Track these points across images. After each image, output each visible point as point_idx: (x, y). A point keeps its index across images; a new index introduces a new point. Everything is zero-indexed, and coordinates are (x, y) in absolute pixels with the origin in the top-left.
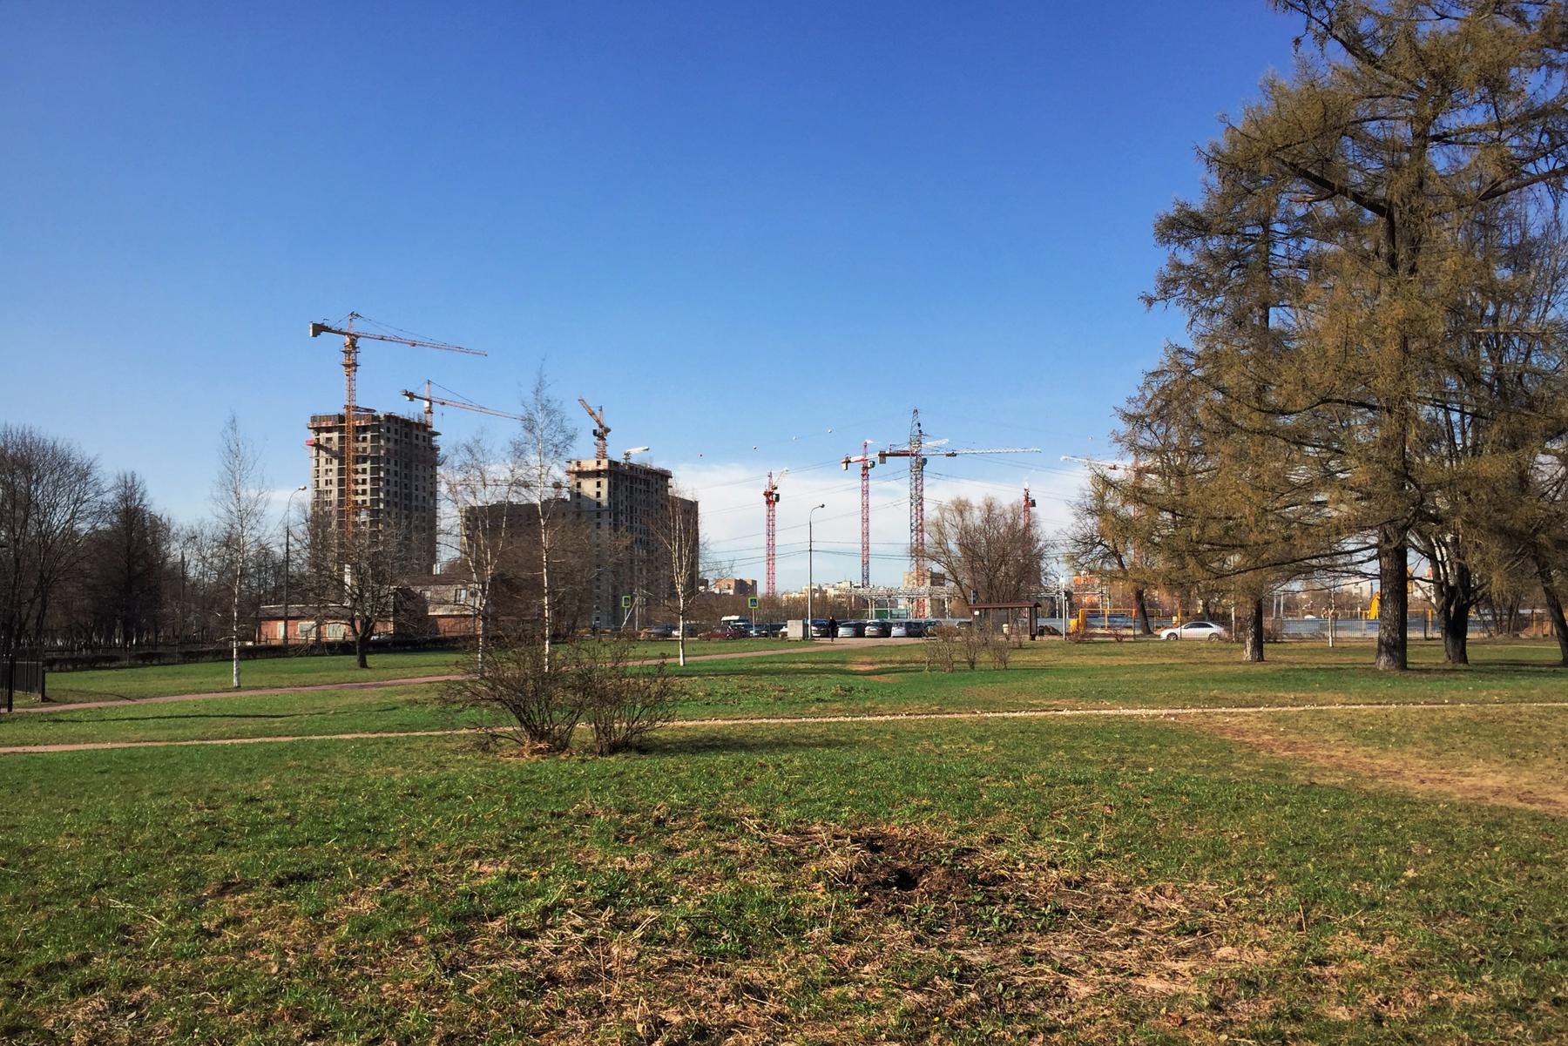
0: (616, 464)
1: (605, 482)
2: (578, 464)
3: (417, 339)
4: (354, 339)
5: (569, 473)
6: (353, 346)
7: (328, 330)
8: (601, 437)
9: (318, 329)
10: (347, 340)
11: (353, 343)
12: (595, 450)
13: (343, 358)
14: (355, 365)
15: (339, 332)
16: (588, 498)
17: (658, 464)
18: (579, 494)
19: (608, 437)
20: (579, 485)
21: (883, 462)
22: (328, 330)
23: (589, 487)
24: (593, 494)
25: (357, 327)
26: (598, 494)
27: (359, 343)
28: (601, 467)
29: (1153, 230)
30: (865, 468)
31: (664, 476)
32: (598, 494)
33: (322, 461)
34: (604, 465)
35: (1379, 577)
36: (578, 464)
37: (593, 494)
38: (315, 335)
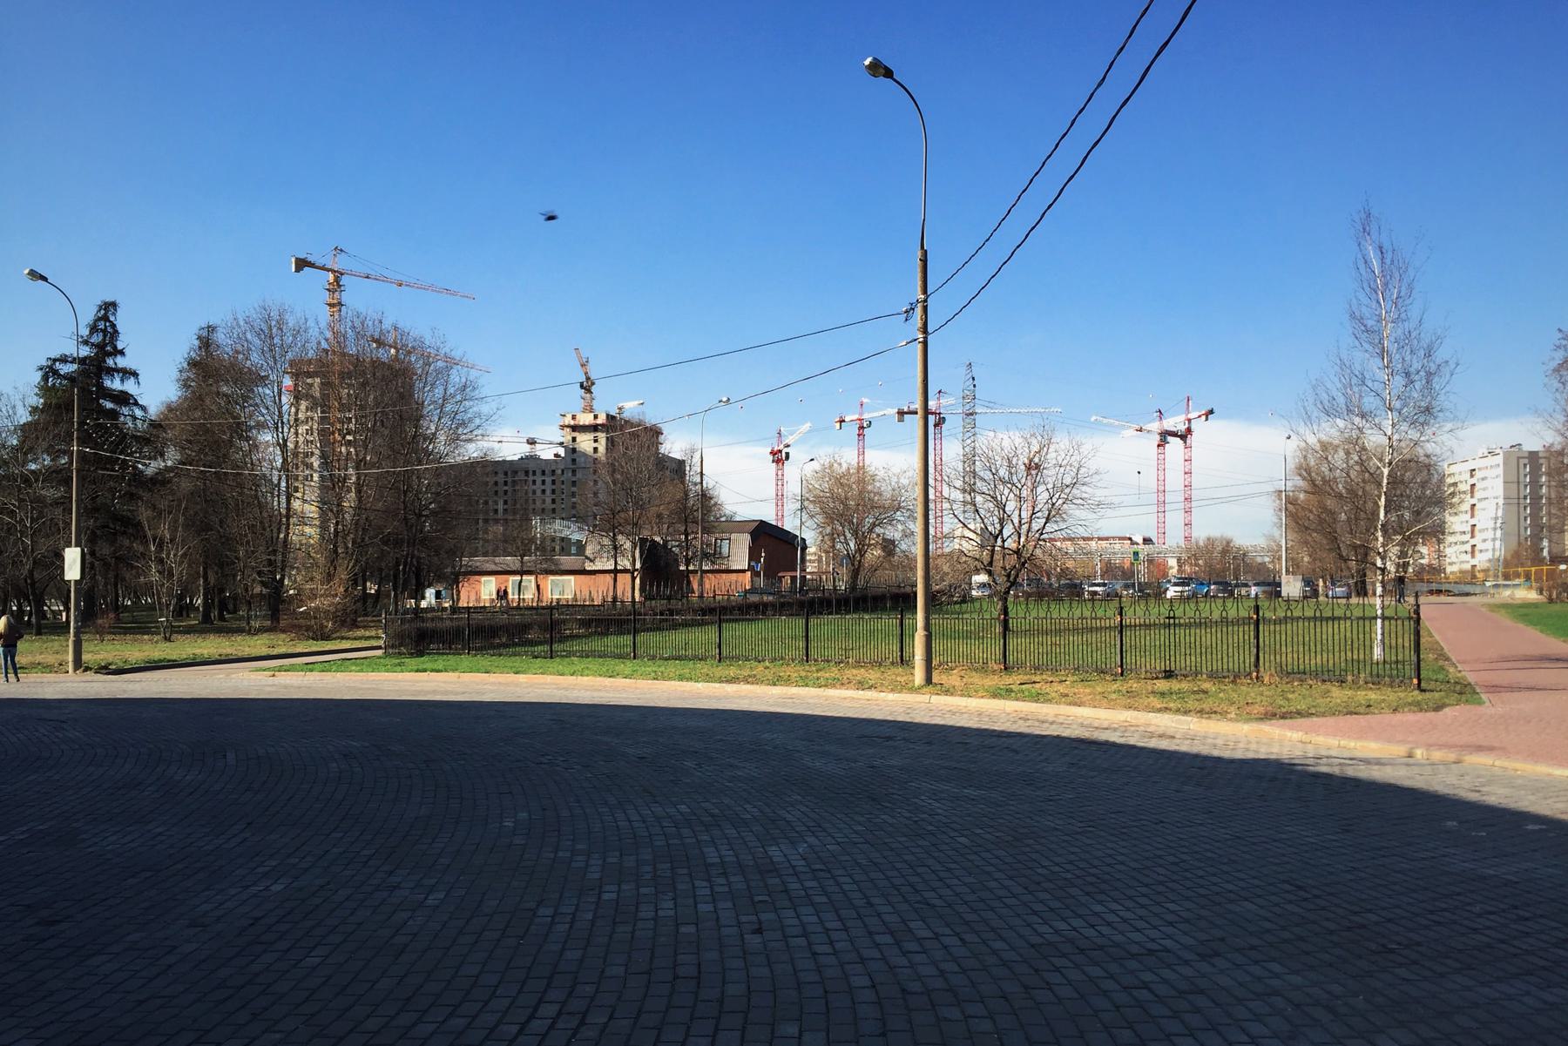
0: (613, 418)
1: (602, 436)
2: (574, 417)
3: (404, 279)
4: (338, 275)
5: (563, 427)
6: (336, 286)
7: (312, 265)
8: (588, 390)
9: (302, 264)
10: (331, 277)
11: (337, 280)
12: (582, 404)
13: (327, 297)
14: (340, 304)
15: (323, 268)
16: (585, 455)
17: (651, 419)
18: (574, 450)
19: (593, 389)
20: (574, 439)
21: (901, 420)
22: (312, 265)
23: (585, 443)
24: (590, 450)
25: (340, 263)
26: (596, 449)
27: (344, 280)
28: (599, 421)
29: (175, 374)
30: (862, 428)
31: (655, 432)
32: (596, 449)
33: (303, 407)
34: (602, 420)
35: (861, 468)
36: (574, 417)
37: (590, 450)
38: (298, 270)
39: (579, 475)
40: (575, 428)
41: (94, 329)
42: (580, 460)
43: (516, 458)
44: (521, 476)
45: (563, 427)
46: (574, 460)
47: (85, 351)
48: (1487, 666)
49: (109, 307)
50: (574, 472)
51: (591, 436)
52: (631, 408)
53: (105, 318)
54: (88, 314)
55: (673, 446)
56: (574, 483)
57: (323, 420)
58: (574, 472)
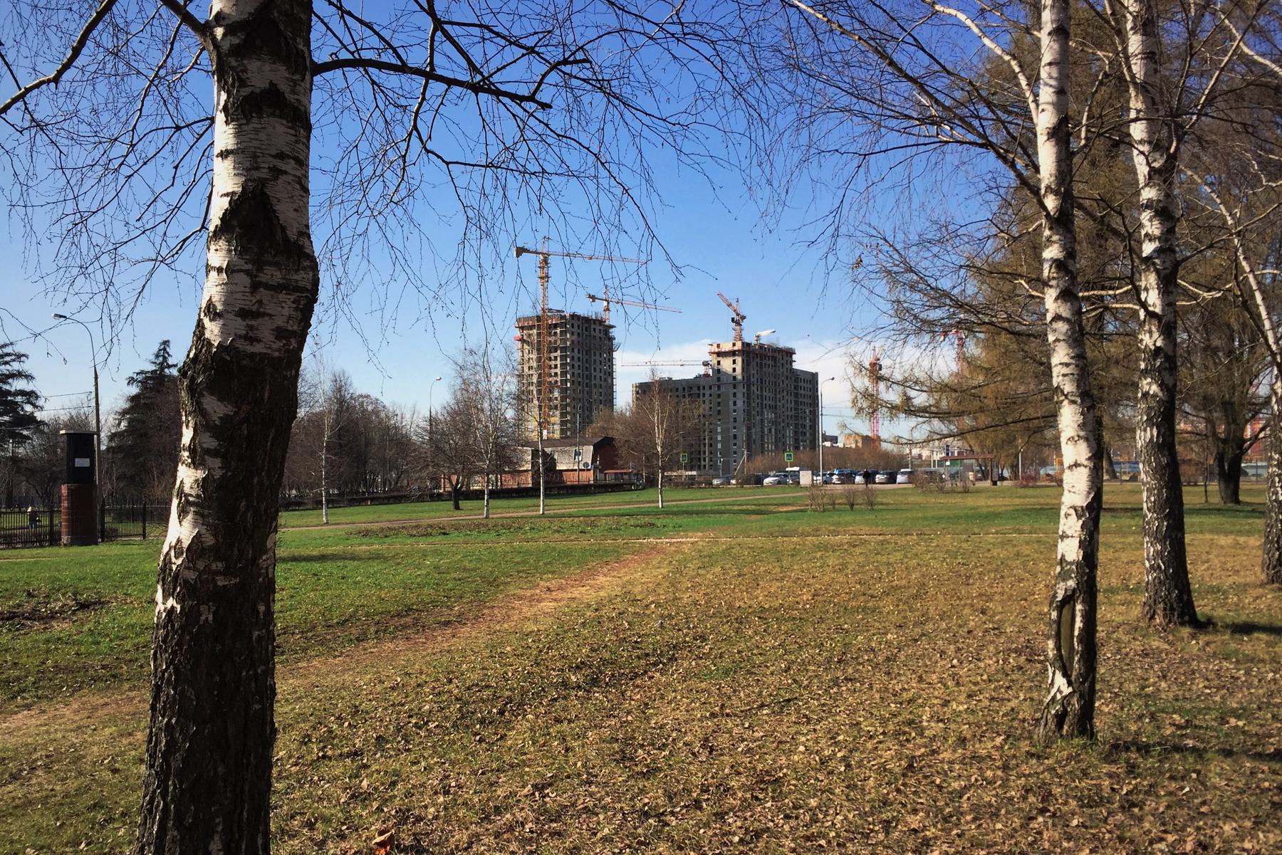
1: (739, 360)
2: (718, 346)
5: (711, 353)
7: (527, 251)
8: (738, 323)
12: (733, 334)
13: (539, 273)
15: (536, 252)
17: (783, 343)
19: (744, 323)
20: (719, 363)
22: (527, 251)
23: (727, 365)
24: (730, 370)
26: (734, 370)
27: (551, 259)
31: (789, 353)
32: (734, 370)
36: (718, 346)
37: (730, 370)
39: (723, 389)
40: (719, 354)
41: (157, 356)
42: (724, 379)
43: (692, 377)
44: (695, 390)
45: (711, 353)
46: (719, 379)
47: (152, 368)
48: (772, 508)
49: (166, 343)
50: (719, 387)
51: (731, 359)
52: (767, 336)
53: (164, 349)
54: (155, 347)
55: (802, 363)
56: (719, 396)
57: (539, 359)
58: (719, 387)
